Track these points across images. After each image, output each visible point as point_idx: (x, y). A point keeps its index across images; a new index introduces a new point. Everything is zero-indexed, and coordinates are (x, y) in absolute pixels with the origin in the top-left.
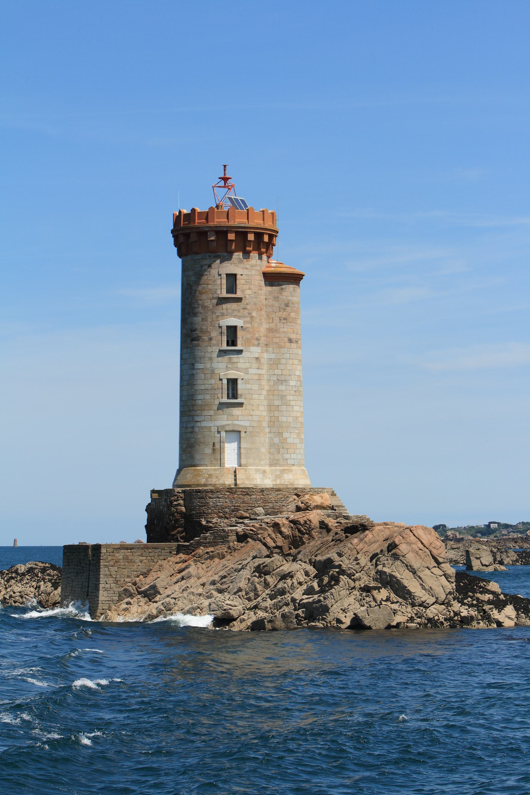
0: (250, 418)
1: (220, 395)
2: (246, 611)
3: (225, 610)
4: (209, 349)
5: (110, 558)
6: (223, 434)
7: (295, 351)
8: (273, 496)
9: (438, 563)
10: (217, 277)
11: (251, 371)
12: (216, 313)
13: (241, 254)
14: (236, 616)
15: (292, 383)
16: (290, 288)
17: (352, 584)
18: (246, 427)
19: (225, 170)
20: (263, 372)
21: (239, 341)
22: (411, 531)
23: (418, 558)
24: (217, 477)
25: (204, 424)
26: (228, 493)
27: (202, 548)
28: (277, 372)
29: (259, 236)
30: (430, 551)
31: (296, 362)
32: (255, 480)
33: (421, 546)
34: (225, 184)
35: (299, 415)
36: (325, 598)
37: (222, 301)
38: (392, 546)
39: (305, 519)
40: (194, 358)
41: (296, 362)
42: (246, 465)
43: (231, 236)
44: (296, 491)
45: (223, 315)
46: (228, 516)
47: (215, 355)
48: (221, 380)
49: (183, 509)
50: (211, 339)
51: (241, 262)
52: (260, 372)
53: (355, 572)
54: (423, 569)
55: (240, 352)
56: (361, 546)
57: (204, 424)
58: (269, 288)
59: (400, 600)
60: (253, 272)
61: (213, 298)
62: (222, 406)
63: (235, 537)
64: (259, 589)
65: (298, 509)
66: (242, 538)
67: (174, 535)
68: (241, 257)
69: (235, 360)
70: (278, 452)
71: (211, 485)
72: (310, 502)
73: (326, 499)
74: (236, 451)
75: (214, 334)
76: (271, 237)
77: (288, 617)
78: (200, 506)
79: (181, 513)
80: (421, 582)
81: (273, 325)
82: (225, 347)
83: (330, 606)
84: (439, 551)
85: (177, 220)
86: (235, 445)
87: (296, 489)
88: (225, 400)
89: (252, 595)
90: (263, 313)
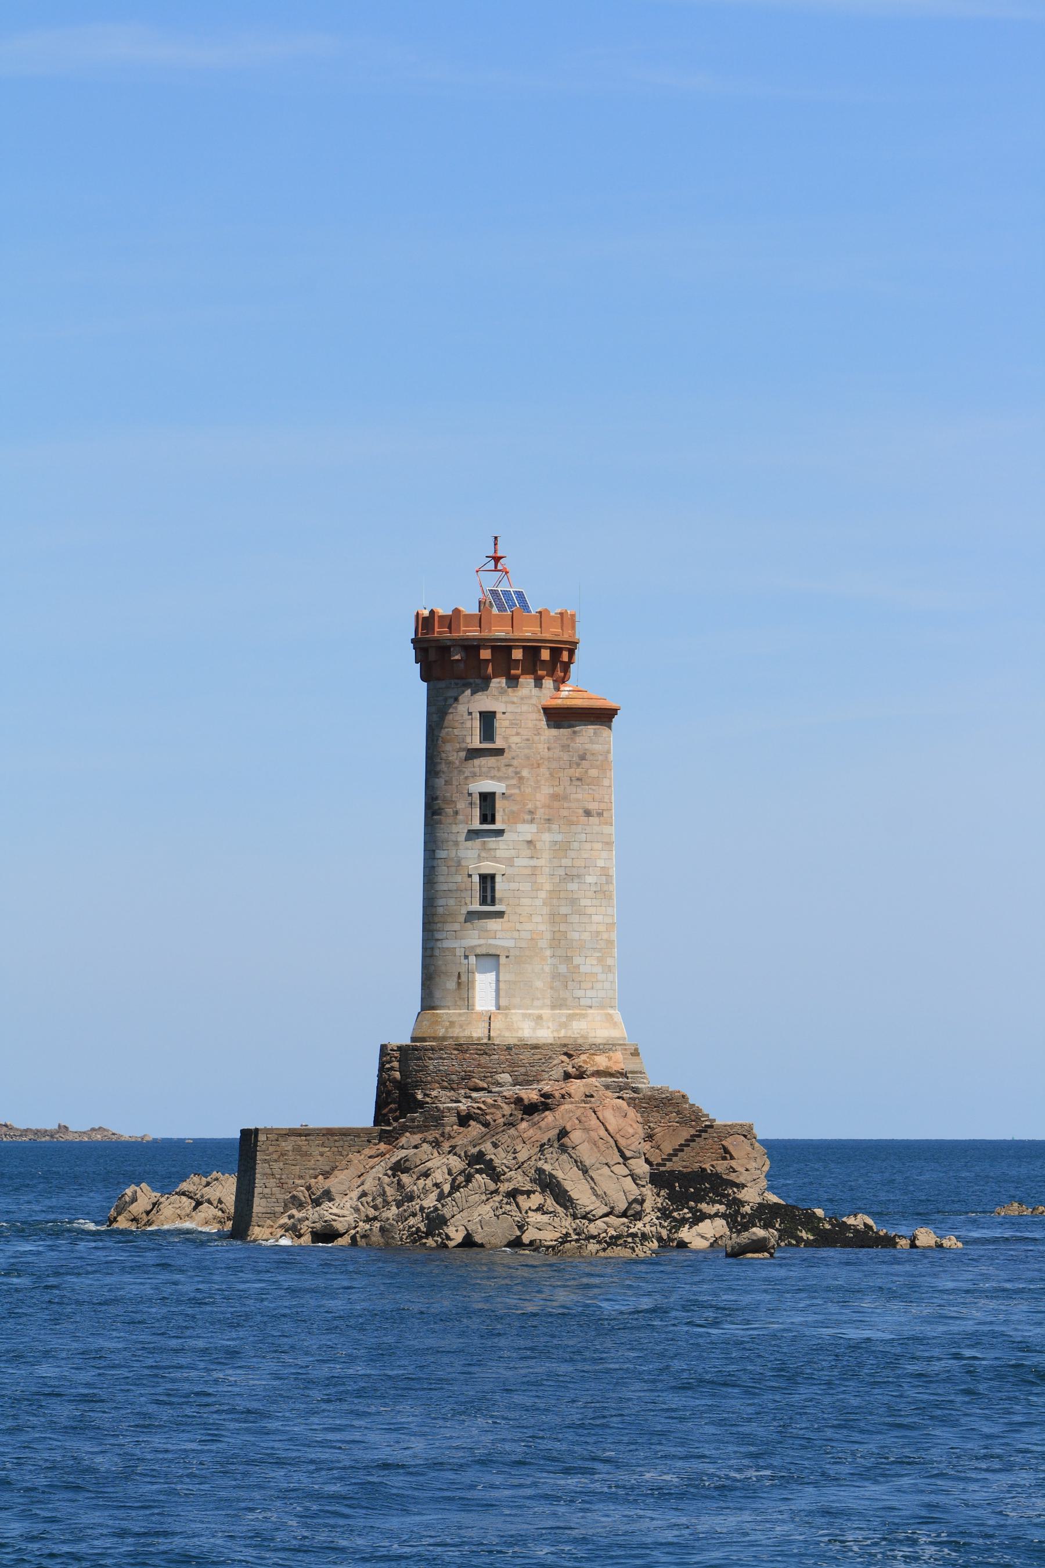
0: (516, 934)
1: (468, 900)
2: (361, 1224)
3: (326, 1221)
4: (455, 829)
5: (271, 1149)
6: (472, 959)
7: (596, 829)
8: (525, 1057)
9: (625, 1158)
10: (466, 716)
11: (518, 862)
12: (464, 773)
13: (503, 680)
14: (342, 1230)
15: (589, 879)
16: (589, 730)
17: (492, 1186)
18: (508, 949)
19: (496, 544)
20: (541, 862)
21: (498, 817)
22: (595, 1112)
23: (596, 1150)
24: (461, 1026)
25: (446, 944)
26: (456, 1052)
27: (408, 1134)
28: (565, 862)
29: (532, 651)
30: (615, 1142)
31: (598, 846)
32: (520, 1032)
33: (602, 1132)
34: (496, 566)
35: (602, 928)
36: (443, 1206)
37: (474, 754)
38: (563, 1133)
39: (563, 1092)
40: (435, 842)
41: (598, 846)
42: (507, 1008)
43: (485, 654)
44: (565, 1049)
45: (474, 775)
46: (455, 1086)
47: (462, 837)
48: (470, 876)
49: (397, 1075)
50: (456, 813)
51: (502, 692)
52: (534, 862)
53: (506, 1170)
54: (599, 1166)
55: (500, 833)
56: (531, 1132)
57: (446, 944)
58: (554, 732)
59: (560, 1209)
60: (525, 708)
61: (461, 750)
62: (472, 916)
63: (455, 1119)
64: (388, 1194)
65: (567, 1076)
66: (464, 1120)
67: (385, 1115)
68: (504, 685)
69: (492, 845)
70: (565, 986)
71: (452, 1037)
72: (586, 1066)
73: (618, 1061)
74: (494, 985)
75: (461, 805)
76: (571, 652)
77: (388, 1230)
78: (416, 1071)
79: (394, 1081)
80: (593, 1185)
81: (559, 790)
82: (476, 825)
83: (448, 1216)
84: (629, 1142)
85: (426, 623)
86: (491, 976)
87: (565, 1045)
88: (476, 907)
89: (379, 1200)
90: (543, 770)
